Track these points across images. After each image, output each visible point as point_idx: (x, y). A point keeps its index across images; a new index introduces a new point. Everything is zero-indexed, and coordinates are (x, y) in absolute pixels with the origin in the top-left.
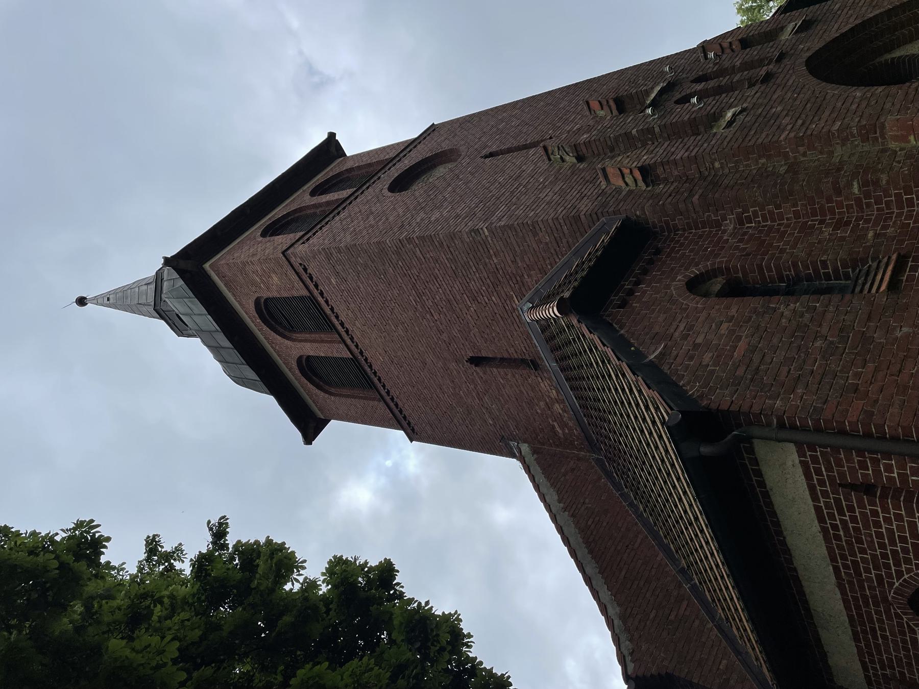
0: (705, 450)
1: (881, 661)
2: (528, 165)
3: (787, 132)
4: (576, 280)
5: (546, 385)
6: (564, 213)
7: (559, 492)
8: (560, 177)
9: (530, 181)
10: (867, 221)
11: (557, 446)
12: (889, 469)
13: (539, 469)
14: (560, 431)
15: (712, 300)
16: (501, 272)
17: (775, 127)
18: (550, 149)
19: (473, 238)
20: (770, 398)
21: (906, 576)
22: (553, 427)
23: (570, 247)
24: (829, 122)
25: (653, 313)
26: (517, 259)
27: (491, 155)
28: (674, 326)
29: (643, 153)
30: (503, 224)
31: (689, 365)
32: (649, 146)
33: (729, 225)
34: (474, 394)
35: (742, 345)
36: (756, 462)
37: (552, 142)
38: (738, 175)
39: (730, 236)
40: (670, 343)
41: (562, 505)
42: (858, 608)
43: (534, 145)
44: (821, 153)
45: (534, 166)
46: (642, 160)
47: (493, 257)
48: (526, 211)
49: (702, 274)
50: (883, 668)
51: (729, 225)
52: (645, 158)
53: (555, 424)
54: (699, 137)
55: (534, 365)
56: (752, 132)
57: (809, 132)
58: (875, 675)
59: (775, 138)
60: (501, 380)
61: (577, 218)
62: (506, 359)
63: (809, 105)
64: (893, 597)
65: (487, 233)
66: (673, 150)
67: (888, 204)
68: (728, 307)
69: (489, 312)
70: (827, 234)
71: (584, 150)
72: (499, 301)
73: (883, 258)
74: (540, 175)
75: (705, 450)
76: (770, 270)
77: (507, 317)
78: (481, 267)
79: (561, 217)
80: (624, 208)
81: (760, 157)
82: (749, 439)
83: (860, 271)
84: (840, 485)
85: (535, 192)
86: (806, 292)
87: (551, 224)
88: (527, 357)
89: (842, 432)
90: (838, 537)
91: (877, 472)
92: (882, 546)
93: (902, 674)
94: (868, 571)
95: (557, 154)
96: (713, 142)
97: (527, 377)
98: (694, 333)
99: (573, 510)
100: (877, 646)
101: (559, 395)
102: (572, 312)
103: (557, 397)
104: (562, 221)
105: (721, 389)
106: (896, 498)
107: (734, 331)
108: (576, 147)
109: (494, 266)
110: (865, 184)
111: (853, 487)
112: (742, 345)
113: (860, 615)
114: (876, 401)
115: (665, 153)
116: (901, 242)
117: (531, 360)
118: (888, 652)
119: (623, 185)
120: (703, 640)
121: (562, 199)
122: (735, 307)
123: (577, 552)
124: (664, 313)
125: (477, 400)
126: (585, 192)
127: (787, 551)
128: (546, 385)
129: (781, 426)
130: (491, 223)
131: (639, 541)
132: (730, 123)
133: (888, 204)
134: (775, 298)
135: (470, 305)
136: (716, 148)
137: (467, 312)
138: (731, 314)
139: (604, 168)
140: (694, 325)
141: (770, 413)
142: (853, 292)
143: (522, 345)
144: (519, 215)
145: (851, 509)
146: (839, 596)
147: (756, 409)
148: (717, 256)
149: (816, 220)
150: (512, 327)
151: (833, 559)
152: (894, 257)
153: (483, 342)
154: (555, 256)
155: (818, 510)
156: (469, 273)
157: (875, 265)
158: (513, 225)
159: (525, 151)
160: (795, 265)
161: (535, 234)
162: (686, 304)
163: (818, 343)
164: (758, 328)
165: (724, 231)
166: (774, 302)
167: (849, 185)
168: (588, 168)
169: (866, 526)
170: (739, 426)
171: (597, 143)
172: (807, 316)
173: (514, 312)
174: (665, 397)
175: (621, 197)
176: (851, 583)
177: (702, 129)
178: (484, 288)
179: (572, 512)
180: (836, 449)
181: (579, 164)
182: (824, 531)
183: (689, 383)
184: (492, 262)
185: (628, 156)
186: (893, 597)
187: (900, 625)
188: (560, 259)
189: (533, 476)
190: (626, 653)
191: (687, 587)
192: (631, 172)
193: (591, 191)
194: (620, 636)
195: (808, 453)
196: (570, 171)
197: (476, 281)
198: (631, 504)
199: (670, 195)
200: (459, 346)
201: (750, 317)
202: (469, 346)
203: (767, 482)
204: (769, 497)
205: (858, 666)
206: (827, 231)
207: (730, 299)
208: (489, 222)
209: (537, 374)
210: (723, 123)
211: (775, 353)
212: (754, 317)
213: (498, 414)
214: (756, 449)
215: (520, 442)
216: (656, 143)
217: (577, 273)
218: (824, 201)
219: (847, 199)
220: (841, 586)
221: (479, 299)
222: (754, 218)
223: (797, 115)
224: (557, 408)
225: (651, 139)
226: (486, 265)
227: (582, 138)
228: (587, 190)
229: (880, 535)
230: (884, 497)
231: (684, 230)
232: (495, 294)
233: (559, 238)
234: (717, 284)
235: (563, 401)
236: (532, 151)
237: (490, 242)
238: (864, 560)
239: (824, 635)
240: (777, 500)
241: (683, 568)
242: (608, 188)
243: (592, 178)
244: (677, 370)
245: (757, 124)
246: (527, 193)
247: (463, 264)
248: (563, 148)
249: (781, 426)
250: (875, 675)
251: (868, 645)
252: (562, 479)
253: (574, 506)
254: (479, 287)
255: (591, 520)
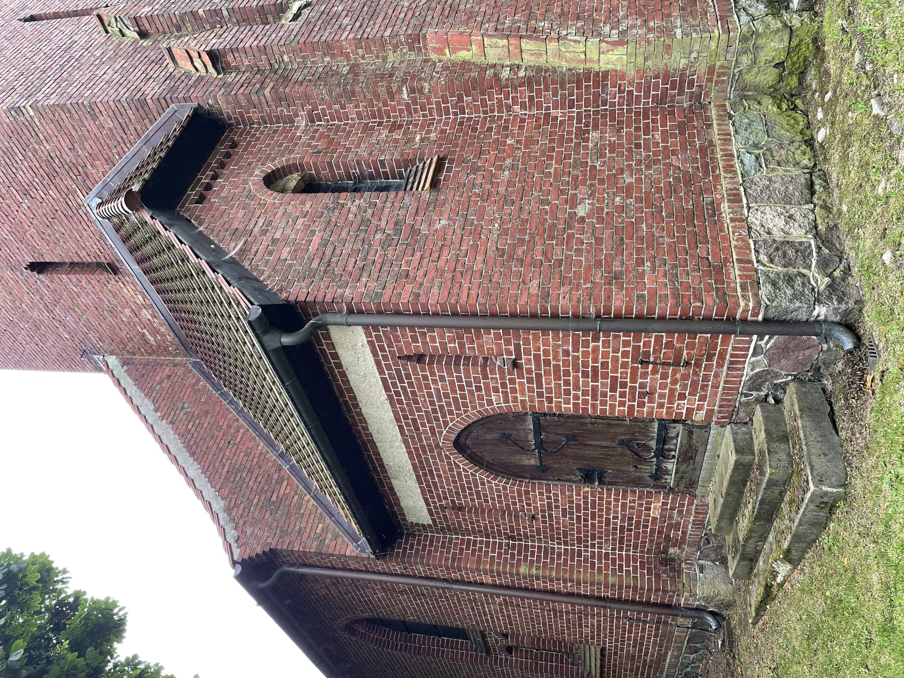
0: (286, 340)
1: (438, 495)
2: (80, 36)
3: (347, 33)
4: (147, 172)
5: (130, 290)
6: (127, 95)
7: (154, 402)
8: (120, 53)
9: (84, 54)
10: (415, 126)
11: (150, 354)
12: (433, 339)
13: (130, 381)
14: (152, 339)
15: (289, 195)
16: (57, 160)
17: (336, 27)
18: (105, 18)
19: (14, 118)
20: (340, 287)
21: (450, 425)
22: (143, 335)
23: (138, 135)
24: (382, 28)
25: (232, 209)
26: (76, 145)
27: (32, 18)
28: (253, 222)
29: (211, 37)
30: (51, 103)
31: (269, 260)
32: (218, 29)
33: (302, 122)
34: (41, 306)
35: (316, 239)
36: (332, 346)
37: (107, 11)
38: (306, 71)
39: (303, 133)
40: (249, 239)
41: (159, 414)
42: (419, 456)
43: (86, 12)
44: (377, 57)
45: (88, 37)
46: (211, 44)
47: (44, 142)
48: (81, 89)
49: (278, 169)
50: (440, 500)
51: (302, 122)
52: (214, 43)
53: (145, 331)
54: (268, 27)
55: (113, 269)
56: (316, 29)
57: (365, 36)
58: (435, 507)
59: (337, 38)
60: (74, 288)
61: (143, 102)
62: (77, 263)
63: (366, 8)
64: (443, 443)
65: (32, 113)
66: (242, 36)
67: (430, 110)
68: (303, 203)
69: (47, 209)
70: (384, 136)
71: (147, 25)
72: (59, 195)
73: (427, 159)
74: (96, 48)
75: (286, 340)
76: (339, 168)
77: (71, 213)
78: (30, 154)
79: (124, 99)
80: (194, 95)
81: (325, 55)
82: (324, 326)
83: (410, 171)
84: (399, 358)
85: (91, 68)
86: (370, 190)
87: (113, 107)
88: (103, 260)
89: (398, 313)
90: (400, 402)
91: (425, 343)
92: (432, 403)
93: (453, 501)
94: (423, 425)
95: (115, 26)
96: (281, 34)
97: (106, 283)
98: (272, 228)
99: (171, 416)
100: (435, 484)
101: (146, 300)
102: (143, 208)
103: (144, 303)
104: (126, 105)
105: (298, 282)
106: (475, 364)
107: (309, 226)
108: (136, 20)
109: (46, 153)
110: (412, 90)
111: (409, 358)
112: (316, 239)
113: (421, 462)
114: (421, 284)
115: (234, 39)
116: (440, 146)
117: (108, 264)
118: (442, 487)
119: (194, 71)
120: (302, 511)
121: (124, 78)
122: (310, 202)
123: (177, 458)
124: (243, 209)
125: (46, 313)
126: (151, 74)
127: (364, 421)
128: (130, 290)
129: (351, 312)
130: (37, 101)
131: (240, 435)
132: (296, 17)
133: (430, 110)
134: (344, 194)
135: (21, 200)
136: (283, 40)
137: (18, 209)
138: (306, 210)
139: (170, 48)
140: (272, 221)
141: (340, 301)
142: (405, 190)
143: (95, 247)
144: (72, 93)
145: (408, 377)
146: (405, 450)
147: (329, 298)
148: (291, 152)
149: (375, 122)
150: (80, 226)
151: (398, 420)
152: (435, 159)
153: (45, 244)
154: (123, 145)
155: (384, 380)
156: (13, 161)
157: (421, 165)
158: (65, 105)
159: (77, 18)
160: (359, 163)
161: (94, 118)
162: (264, 200)
163: (378, 236)
164: (329, 222)
165: (297, 128)
166: (343, 198)
167: (400, 91)
168: (154, 46)
169: (420, 389)
170: (315, 315)
171: (161, 19)
172: (370, 211)
173: (80, 208)
174: (246, 293)
175: (191, 82)
176: (412, 437)
177: (271, 19)
178: (37, 180)
179: (170, 419)
180: (394, 327)
181: (143, 41)
182: (390, 398)
183: (269, 277)
184: (43, 148)
185: (195, 38)
186: (443, 443)
187: (449, 464)
188: (129, 149)
189: (124, 389)
190: (231, 541)
191: (286, 468)
192: (200, 57)
193: (158, 72)
194: (226, 528)
195: (374, 334)
196: (132, 48)
197: (26, 171)
198: (231, 402)
199: (242, 86)
200: (12, 250)
201: (323, 213)
202: (26, 250)
203: (343, 363)
204: (346, 376)
205: (422, 503)
206: (385, 133)
207: (304, 195)
208: (34, 99)
209: (117, 279)
210: (290, 15)
211: (344, 246)
212: (326, 212)
213: (75, 327)
214: (332, 335)
215: (106, 354)
216: (225, 27)
217: (148, 164)
218: (381, 105)
219: (399, 104)
220: (405, 442)
221: (31, 193)
222: (324, 116)
223: (355, 16)
224: (146, 314)
225: (220, 22)
226: (36, 152)
227: (143, 11)
228: (153, 72)
229: (430, 395)
230: (448, 364)
231: (259, 124)
232: (53, 187)
233: (124, 124)
234: (293, 180)
235: (151, 307)
236: (85, 19)
237: (38, 124)
238: (420, 417)
239: (395, 483)
240: (352, 377)
241: (282, 452)
242: (176, 71)
243: (158, 59)
244: (258, 265)
245: (320, 21)
246: (81, 68)
247: (5, 150)
248: (121, 19)
249: (351, 312)
250: (435, 507)
251: (428, 486)
252: (157, 388)
253: (172, 413)
254: (32, 180)
255: (191, 423)
